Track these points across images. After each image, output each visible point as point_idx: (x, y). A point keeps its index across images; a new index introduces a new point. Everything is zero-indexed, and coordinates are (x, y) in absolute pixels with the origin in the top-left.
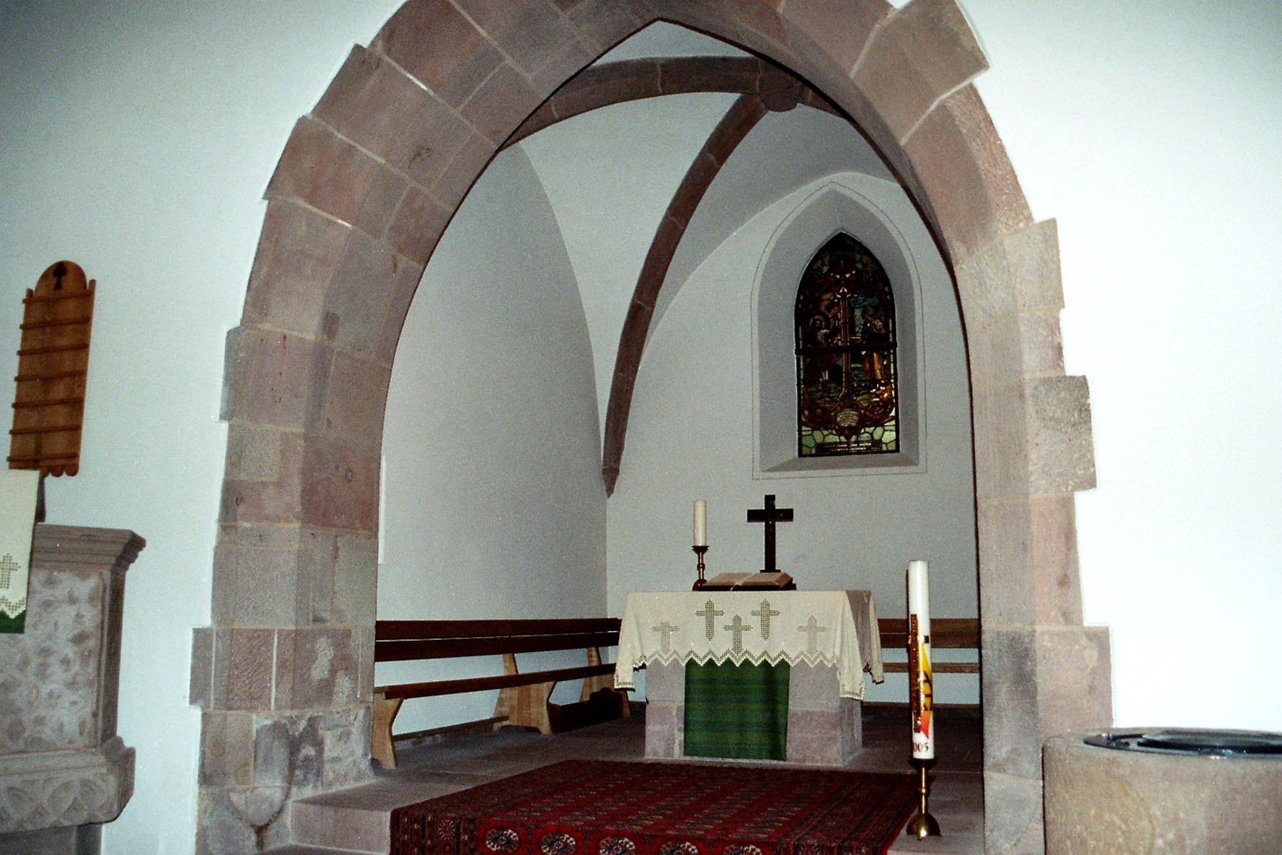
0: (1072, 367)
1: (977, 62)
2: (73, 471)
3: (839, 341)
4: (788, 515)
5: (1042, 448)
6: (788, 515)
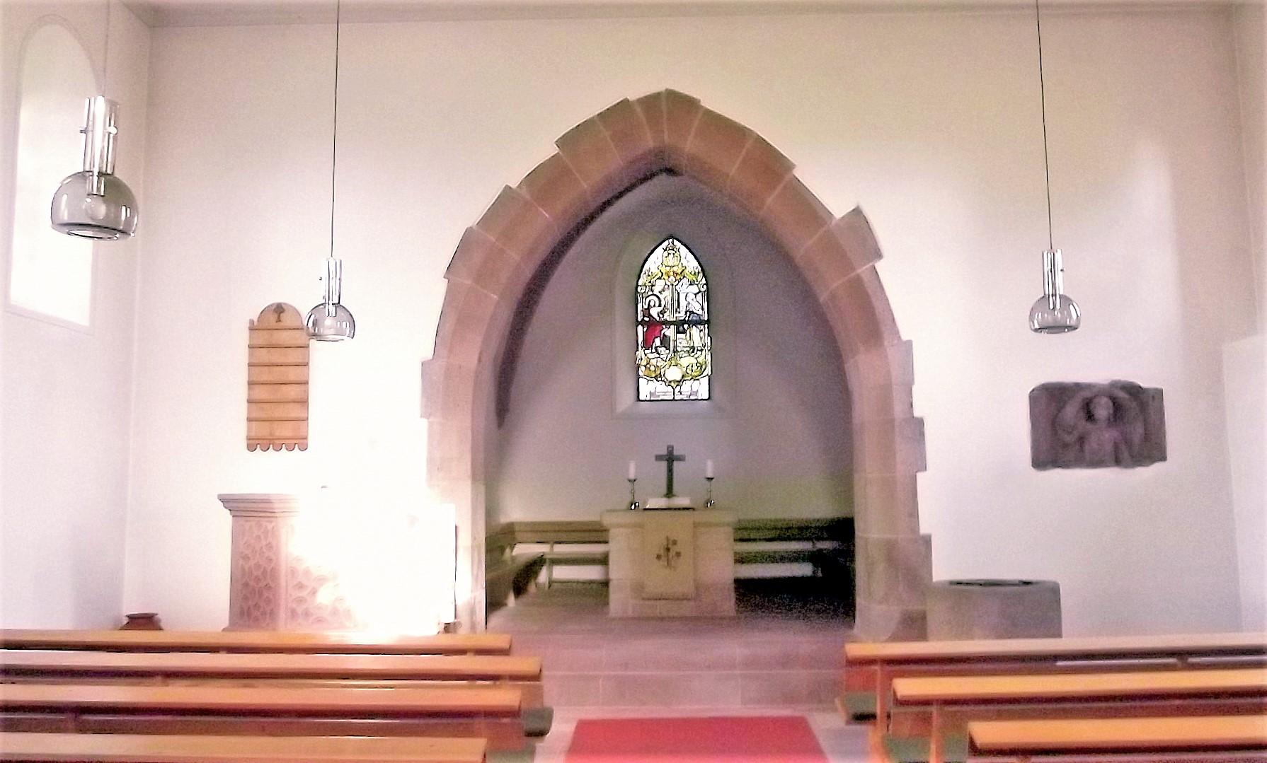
0: (917, 413)
1: (878, 255)
2: (304, 448)
3: (667, 316)
4: (681, 459)
5: (902, 450)
6: (681, 459)
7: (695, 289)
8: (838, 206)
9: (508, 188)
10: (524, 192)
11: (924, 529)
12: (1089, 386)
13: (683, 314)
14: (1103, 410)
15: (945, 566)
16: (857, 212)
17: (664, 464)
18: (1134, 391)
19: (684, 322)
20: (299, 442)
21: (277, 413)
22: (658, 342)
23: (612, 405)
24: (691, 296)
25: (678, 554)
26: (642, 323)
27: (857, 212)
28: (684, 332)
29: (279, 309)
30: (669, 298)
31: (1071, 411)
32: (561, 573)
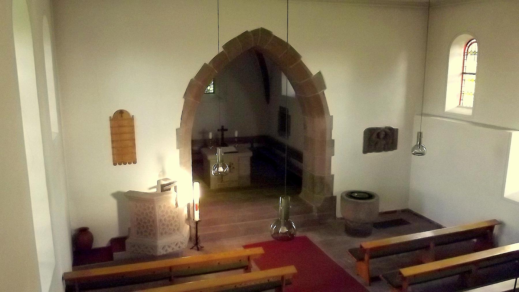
4: (226, 130)
6: (226, 130)
8: (314, 71)
10: (211, 66)
11: (332, 173)
15: (340, 187)
16: (320, 73)
18: (391, 129)
21: (124, 150)
23: (403, 266)
27: (320, 73)
29: (121, 112)
31: (375, 135)
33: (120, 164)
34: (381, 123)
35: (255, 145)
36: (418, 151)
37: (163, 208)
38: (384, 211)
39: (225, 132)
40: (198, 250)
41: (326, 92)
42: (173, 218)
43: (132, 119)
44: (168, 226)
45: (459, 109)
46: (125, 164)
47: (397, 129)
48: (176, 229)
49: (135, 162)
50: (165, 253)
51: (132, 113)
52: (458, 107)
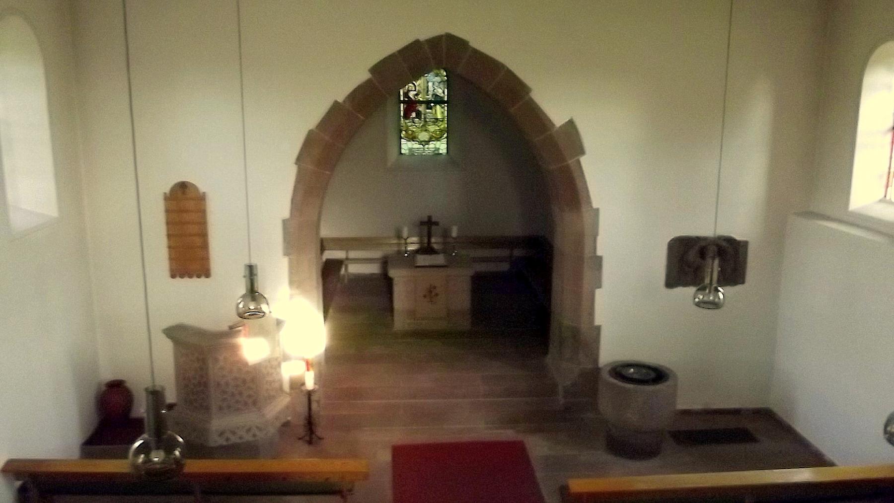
0: (599, 253)
4: (436, 224)
5: (587, 274)
7: (438, 79)
8: (558, 117)
9: (336, 102)
11: (597, 322)
12: (705, 239)
13: (430, 96)
14: (712, 249)
15: (609, 352)
16: (571, 123)
17: (425, 228)
18: (730, 241)
19: (431, 102)
20: (205, 272)
21: (189, 253)
22: (414, 115)
24: (437, 84)
25: (437, 295)
26: (404, 102)
27: (571, 123)
28: (431, 108)
29: (183, 187)
30: (422, 85)
31: (692, 255)
32: (354, 269)
33: (182, 276)
34: (703, 227)
35: (517, 253)
36: (705, 299)
37: (221, 363)
38: (715, 407)
39: (434, 228)
40: (310, 442)
41: (584, 160)
42: (244, 381)
43: (201, 199)
44: (233, 395)
45: (882, 206)
46: (191, 277)
47: (745, 244)
48: (250, 401)
49: (208, 275)
50: (225, 443)
51: (202, 188)
52: (880, 201)
